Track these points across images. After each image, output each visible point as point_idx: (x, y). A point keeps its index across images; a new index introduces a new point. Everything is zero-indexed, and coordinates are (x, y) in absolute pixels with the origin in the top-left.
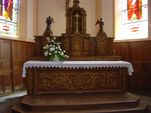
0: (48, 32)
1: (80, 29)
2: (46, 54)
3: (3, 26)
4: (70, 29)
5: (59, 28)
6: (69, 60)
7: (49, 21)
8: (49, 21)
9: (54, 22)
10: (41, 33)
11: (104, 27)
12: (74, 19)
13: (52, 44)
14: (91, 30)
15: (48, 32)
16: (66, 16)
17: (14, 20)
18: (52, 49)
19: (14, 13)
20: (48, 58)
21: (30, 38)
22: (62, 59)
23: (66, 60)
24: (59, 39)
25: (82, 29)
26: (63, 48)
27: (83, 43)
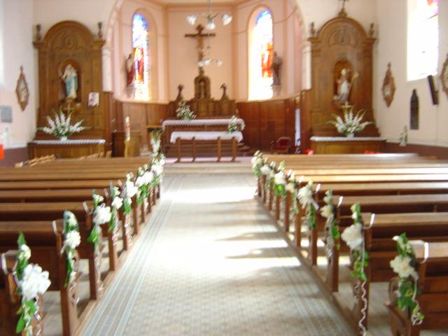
0: (179, 98)
1: (205, 94)
2: (178, 115)
3: (435, 106)
4: (198, 95)
5: (189, 94)
6: (196, 118)
7: (180, 88)
8: (180, 88)
9: (38, 27)
10: (174, 98)
11: (24, 71)
12: (200, 87)
13: (184, 107)
14: (216, 94)
15: (179, 98)
16: (96, 215)
17: (353, 119)
18: (183, 111)
19: (146, 74)
20: (180, 118)
21: (163, 99)
22: (191, 118)
23: (193, 119)
24: (188, 103)
25: (207, 93)
26: (191, 110)
27: (208, 106)
